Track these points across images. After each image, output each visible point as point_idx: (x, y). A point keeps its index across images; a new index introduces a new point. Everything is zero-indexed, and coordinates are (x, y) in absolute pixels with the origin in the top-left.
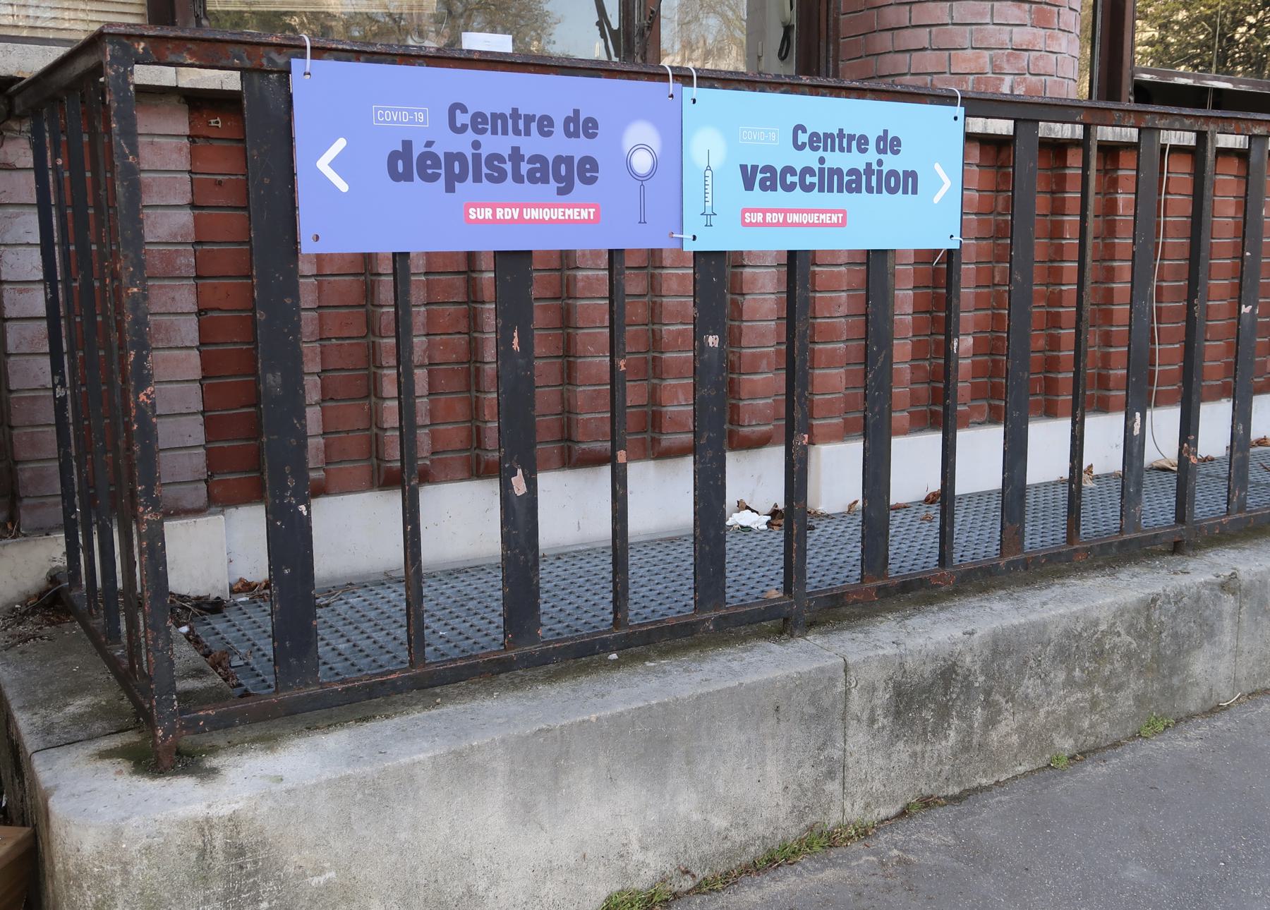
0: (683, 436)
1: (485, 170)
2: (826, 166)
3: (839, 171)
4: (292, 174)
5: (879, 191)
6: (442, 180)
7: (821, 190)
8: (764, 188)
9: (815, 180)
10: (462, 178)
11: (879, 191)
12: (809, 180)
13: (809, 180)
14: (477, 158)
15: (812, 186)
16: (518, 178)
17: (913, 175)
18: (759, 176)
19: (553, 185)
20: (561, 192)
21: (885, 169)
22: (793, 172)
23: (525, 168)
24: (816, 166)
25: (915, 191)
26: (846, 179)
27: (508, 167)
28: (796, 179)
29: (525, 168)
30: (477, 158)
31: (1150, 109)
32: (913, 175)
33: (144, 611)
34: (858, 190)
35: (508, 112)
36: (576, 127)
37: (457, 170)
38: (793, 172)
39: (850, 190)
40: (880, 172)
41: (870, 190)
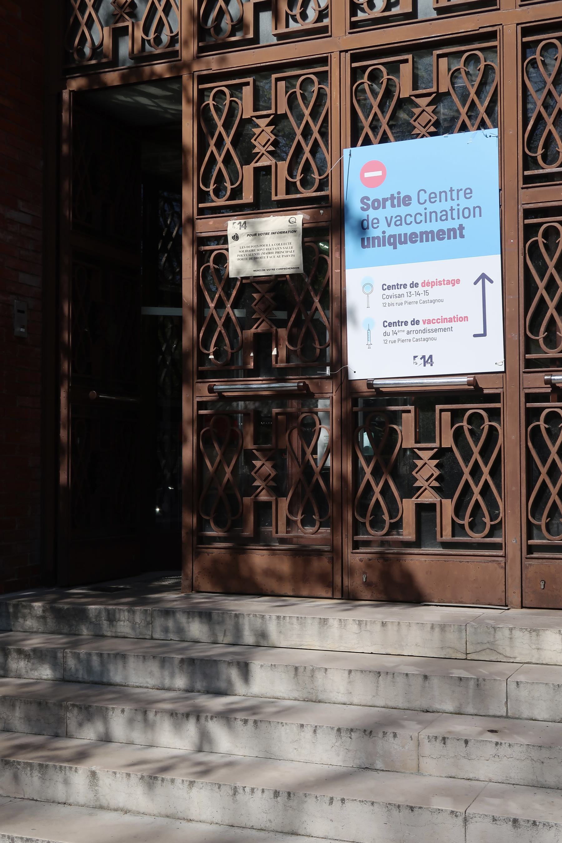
0: (170, 246)
1: (438, 284)
2: (443, 318)
3: (446, 319)
4: (555, 76)
5: (457, 321)
6: (430, 286)
7: (442, 323)
8: (428, 323)
9: (441, 321)
10: (434, 285)
11: (457, 321)
12: (439, 321)
13: (439, 321)
14: (437, 281)
15: (440, 322)
16: (444, 284)
17: (467, 317)
18: (427, 321)
19: (451, 285)
20: (453, 286)
21: (459, 317)
22: (435, 320)
23: (445, 282)
24: (440, 318)
25: (467, 321)
26: (448, 320)
27: (442, 282)
28: (436, 321)
29: (445, 282)
30: (384, 237)
31: (287, 385)
32: (467, 317)
33: (312, 429)
34: (452, 322)
35: (397, 321)
36: (454, 282)
37: (433, 284)
38: (435, 320)
39: (449, 322)
40: (457, 318)
41: (455, 321)
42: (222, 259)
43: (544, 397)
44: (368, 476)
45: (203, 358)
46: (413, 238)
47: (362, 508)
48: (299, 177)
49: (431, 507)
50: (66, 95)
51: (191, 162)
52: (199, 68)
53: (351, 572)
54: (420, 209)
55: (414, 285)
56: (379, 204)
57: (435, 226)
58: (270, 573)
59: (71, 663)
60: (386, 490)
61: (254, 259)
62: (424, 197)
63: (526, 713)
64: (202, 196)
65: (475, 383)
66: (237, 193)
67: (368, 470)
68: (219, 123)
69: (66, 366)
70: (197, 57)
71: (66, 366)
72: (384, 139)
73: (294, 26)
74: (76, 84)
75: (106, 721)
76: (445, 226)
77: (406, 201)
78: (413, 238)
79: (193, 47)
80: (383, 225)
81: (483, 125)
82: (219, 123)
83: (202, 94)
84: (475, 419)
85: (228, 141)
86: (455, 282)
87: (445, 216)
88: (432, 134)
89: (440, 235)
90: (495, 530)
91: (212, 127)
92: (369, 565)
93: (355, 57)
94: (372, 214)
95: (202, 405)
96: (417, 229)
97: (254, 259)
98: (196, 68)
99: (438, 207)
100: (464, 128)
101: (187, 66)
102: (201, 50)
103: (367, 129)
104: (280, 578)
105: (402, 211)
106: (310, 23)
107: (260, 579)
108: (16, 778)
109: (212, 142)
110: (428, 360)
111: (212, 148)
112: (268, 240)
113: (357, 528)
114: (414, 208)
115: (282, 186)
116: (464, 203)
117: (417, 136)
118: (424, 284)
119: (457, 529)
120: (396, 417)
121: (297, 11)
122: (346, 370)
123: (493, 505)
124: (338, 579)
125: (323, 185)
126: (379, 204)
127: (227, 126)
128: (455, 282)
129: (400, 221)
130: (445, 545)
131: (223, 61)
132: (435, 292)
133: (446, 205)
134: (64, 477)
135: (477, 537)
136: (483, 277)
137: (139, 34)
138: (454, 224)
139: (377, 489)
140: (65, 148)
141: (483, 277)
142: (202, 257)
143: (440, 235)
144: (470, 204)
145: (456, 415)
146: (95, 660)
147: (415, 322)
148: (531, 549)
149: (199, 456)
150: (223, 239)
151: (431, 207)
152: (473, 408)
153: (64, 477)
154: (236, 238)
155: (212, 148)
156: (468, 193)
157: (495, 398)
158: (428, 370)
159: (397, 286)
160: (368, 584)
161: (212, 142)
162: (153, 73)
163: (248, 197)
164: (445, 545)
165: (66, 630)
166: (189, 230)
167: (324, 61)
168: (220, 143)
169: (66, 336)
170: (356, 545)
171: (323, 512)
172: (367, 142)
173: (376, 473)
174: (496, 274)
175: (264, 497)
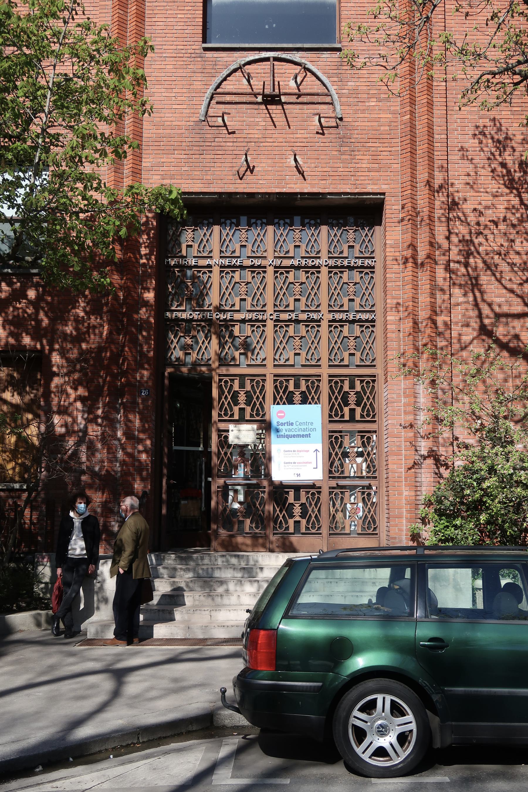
42: (226, 437)
43: (334, 488)
44: (278, 512)
45: (219, 470)
46: (294, 436)
47: (275, 522)
48: (255, 412)
49: (299, 522)
50: (166, 374)
51: (215, 403)
52: (219, 371)
53: (272, 543)
54: (297, 427)
55: (294, 451)
56: (283, 424)
57: (301, 433)
58: (243, 544)
59: (200, 572)
60: (284, 516)
61: (238, 438)
62: (298, 423)
63: (345, 577)
64: (220, 416)
65: (314, 484)
66: (232, 415)
67: (278, 510)
68: (226, 391)
69: (165, 471)
70: (218, 368)
71: (165, 471)
72: (284, 404)
73: (253, 363)
74: (169, 370)
75: (227, 585)
76: (305, 433)
77: (292, 424)
78: (294, 436)
79: (217, 364)
80: (284, 431)
81: (316, 403)
82: (226, 391)
83: (220, 380)
84: (313, 494)
85: (229, 397)
86: (307, 451)
87: (304, 430)
88: (300, 404)
89: (303, 436)
90: (319, 528)
91: (223, 392)
92: (278, 540)
93: (275, 376)
94: (280, 427)
95: (218, 487)
96: (296, 433)
97: (238, 438)
98: (218, 371)
99: (302, 427)
100: (310, 403)
101: (214, 370)
102: (220, 365)
103: (278, 399)
104: (247, 545)
105: (291, 427)
106: (259, 362)
107: (240, 546)
108: (213, 599)
109: (223, 397)
110: (298, 475)
111: (223, 399)
112: (243, 433)
113: (275, 528)
114: (294, 427)
115: (249, 415)
116: (310, 427)
117: (294, 404)
118: (298, 451)
119: (307, 528)
120: (287, 493)
121: (254, 357)
122: (271, 478)
123: (318, 521)
124: (268, 546)
125: (264, 415)
126: (283, 424)
127: (229, 392)
128: (307, 451)
129: (290, 430)
130: (303, 534)
131: (227, 370)
132: (301, 454)
133: (305, 427)
134: (164, 511)
135: (314, 531)
136: (316, 450)
137: (195, 355)
138: (308, 433)
139: (281, 516)
140: (166, 393)
141: (316, 450)
142: (219, 436)
143: (303, 436)
144: (313, 427)
145: (307, 493)
146: (210, 570)
147: (294, 463)
148: (330, 534)
149: (217, 503)
150: (228, 431)
151: (300, 427)
152: (312, 491)
153: (164, 511)
154: (232, 431)
155: (223, 399)
156: (312, 424)
157: (320, 488)
158: (299, 478)
159: (289, 451)
160: (278, 547)
161: (223, 397)
162: (201, 370)
163: (236, 417)
164: (303, 534)
165: (185, 563)
166: (215, 425)
167: (265, 375)
168: (226, 398)
169: (166, 460)
170: (274, 534)
171: (262, 523)
172: (278, 404)
173: (281, 511)
174: (320, 449)
175: (241, 519)
